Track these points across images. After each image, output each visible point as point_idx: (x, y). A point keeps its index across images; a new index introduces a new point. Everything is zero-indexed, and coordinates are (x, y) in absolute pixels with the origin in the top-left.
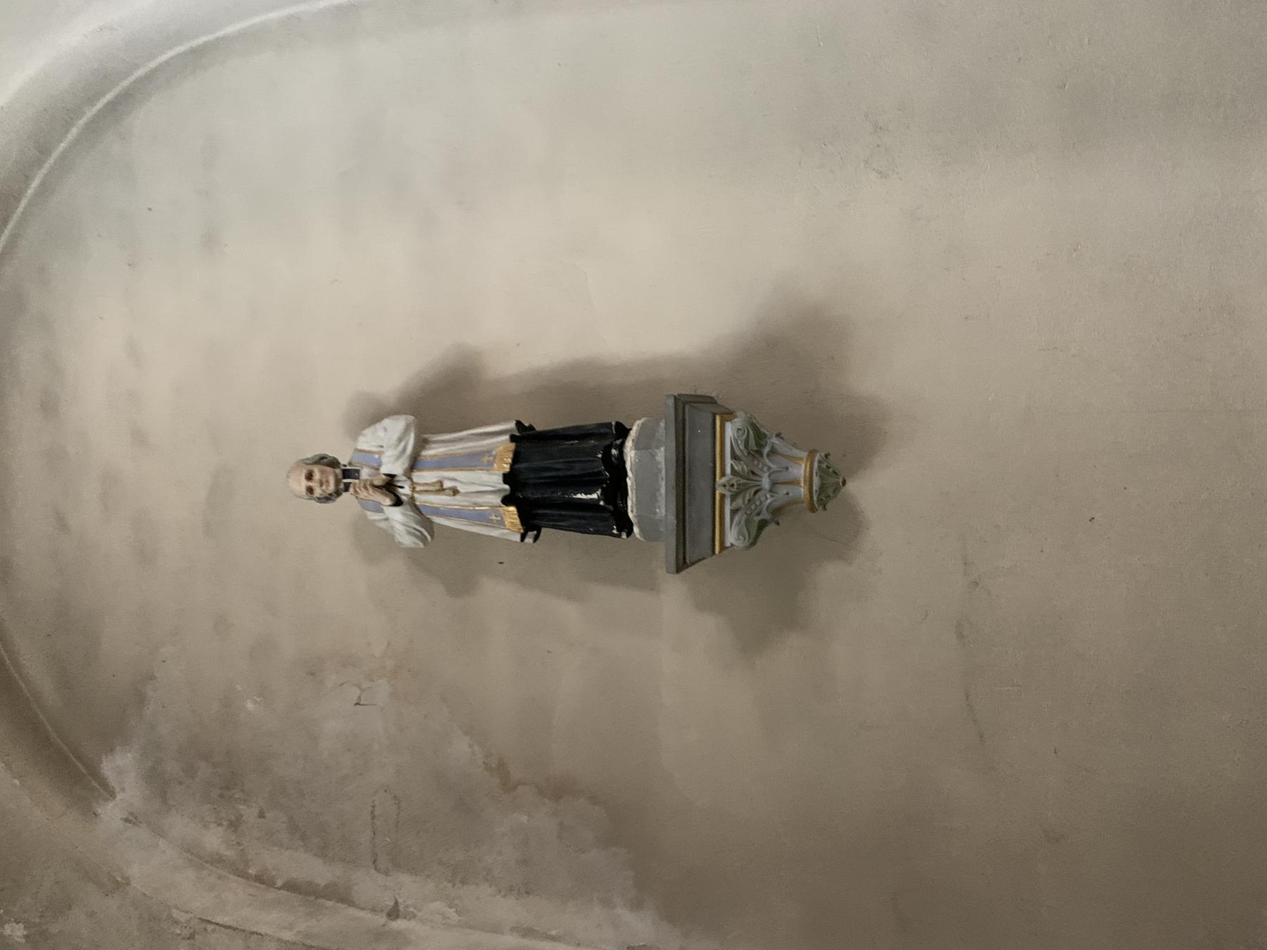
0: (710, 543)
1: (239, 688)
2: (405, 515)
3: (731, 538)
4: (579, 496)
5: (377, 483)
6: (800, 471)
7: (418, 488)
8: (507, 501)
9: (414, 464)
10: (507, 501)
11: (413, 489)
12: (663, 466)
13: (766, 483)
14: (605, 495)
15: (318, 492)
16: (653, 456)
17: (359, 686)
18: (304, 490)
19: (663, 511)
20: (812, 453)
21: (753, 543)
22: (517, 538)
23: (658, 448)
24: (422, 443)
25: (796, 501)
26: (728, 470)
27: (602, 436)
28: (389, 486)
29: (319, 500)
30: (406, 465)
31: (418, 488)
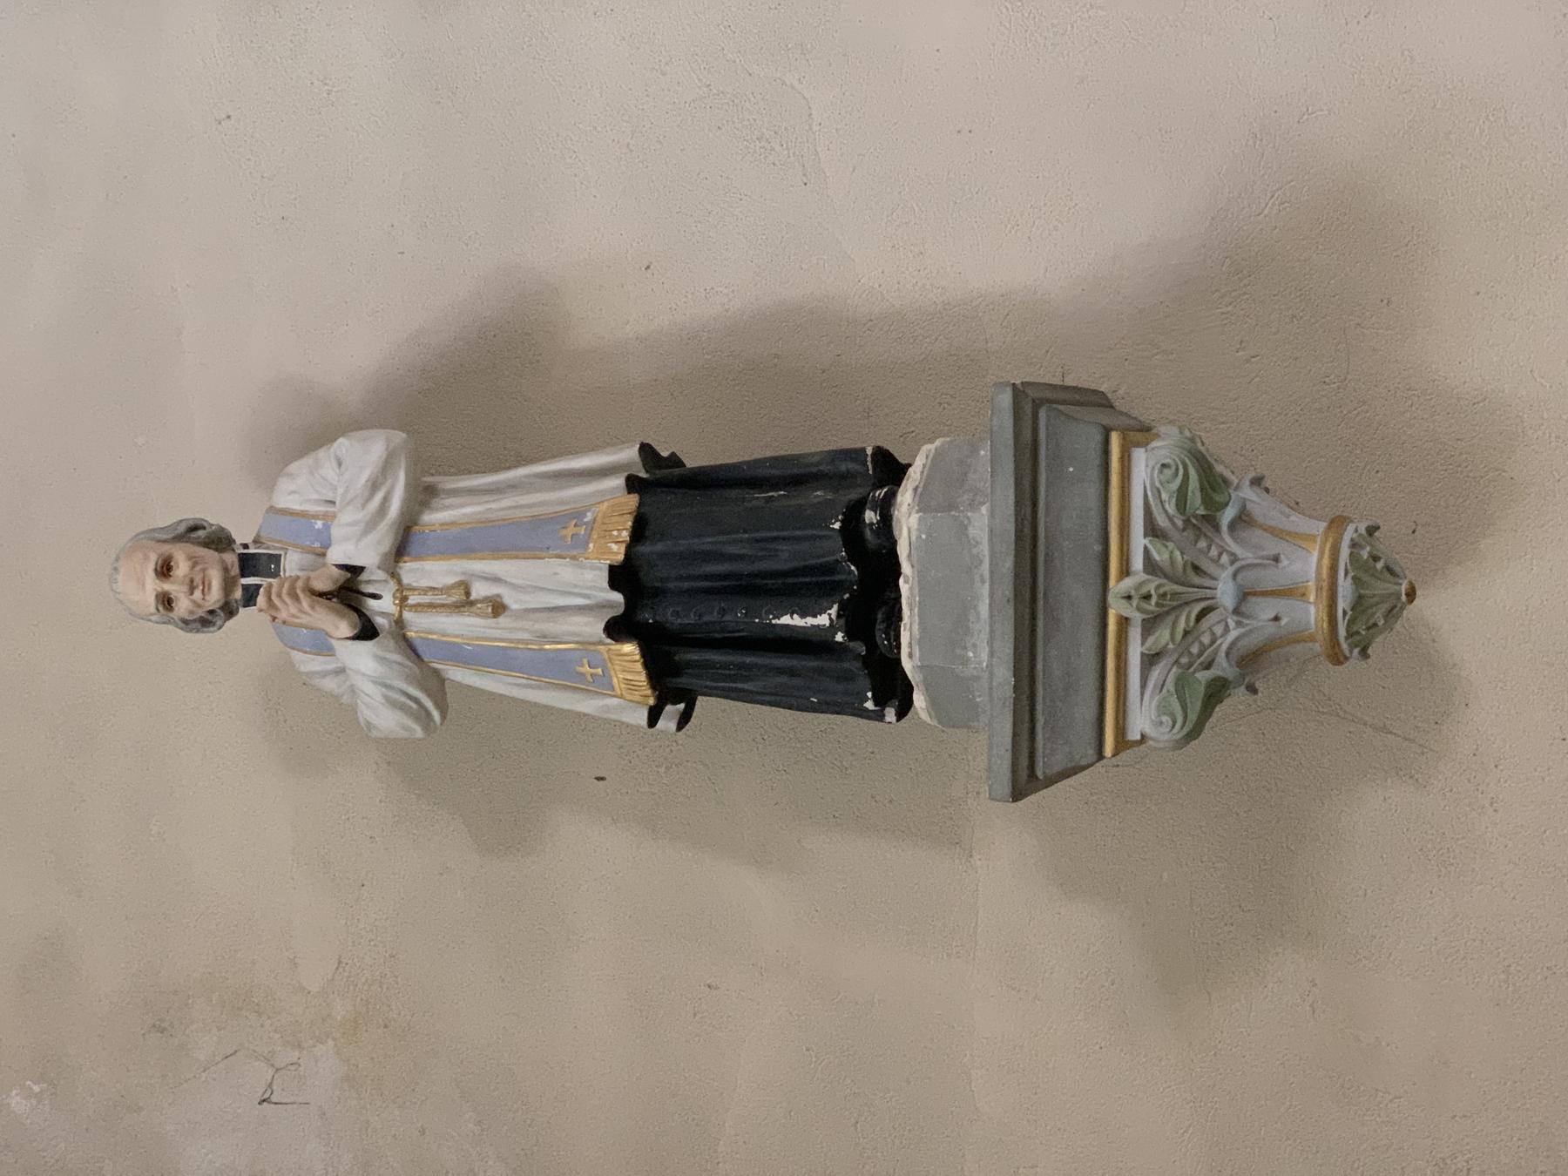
0: (1089, 733)
3: (1141, 721)
4: (786, 620)
5: (320, 586)
6: (1307, 565)
8: (617, 629)
10: (617, 629)
12: (985, 548)
13: (1225, 593)
16: (963, 528)
17: (268, 1060)
19: (984, 655)
20: (1337, 523)
21: (1194, 733)
22: (641, 717)
23: (973, 506)
24: (423, 495)
26: (1138, 563)
28: (348, 592)
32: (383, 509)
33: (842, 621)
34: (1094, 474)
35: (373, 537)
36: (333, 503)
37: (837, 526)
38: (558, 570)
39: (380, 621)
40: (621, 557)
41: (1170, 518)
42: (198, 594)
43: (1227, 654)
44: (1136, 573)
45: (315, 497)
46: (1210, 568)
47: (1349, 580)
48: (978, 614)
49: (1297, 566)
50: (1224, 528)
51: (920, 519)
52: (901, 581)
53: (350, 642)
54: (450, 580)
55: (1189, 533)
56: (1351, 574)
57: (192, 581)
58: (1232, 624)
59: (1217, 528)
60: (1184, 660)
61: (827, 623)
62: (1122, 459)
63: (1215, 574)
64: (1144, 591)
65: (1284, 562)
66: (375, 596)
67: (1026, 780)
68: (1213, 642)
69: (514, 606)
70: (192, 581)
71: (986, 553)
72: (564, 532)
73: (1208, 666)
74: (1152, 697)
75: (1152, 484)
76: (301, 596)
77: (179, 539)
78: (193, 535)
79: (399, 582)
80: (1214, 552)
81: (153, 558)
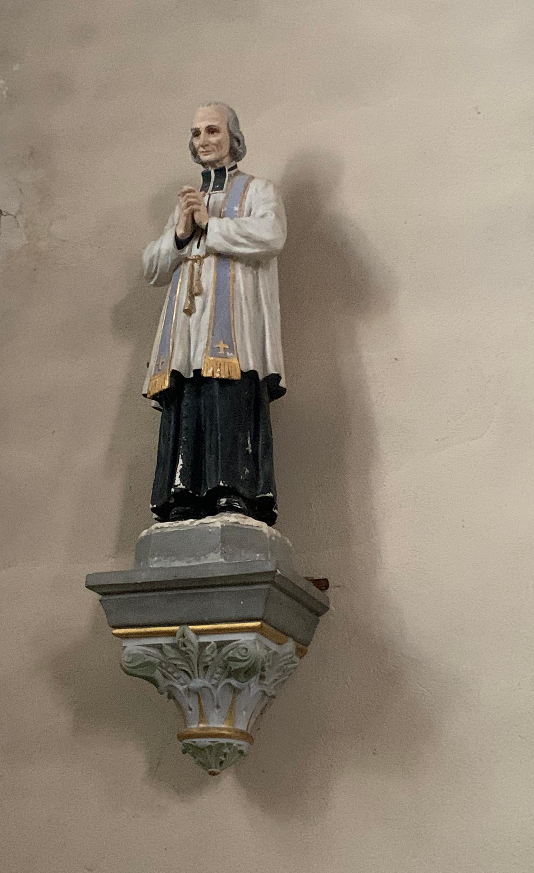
0: (124, 622)
1: (16, 68)
2: (168, 253)
3: (132, 646)
4: (181, 462)
5: (196, 216)
6: (217, 722)
7: (196, 265)
8: (175, 375)
9: (224, 257)
10: (175, 375)
11: (195, 260)
12: (203, 561)
13: (197, 683)
14: (181, 495)
15: (197, 142)
16: (213, 549)
17: (20, 212)
18: (197, 125)
19: (155, 566)
20: (246, 736)
21: (127, 673)
22: (145, 392)
23: (224, 554)
24: (254, 263)
25: (185, 722)
26: (203, 639)
27: (254, 480)
28: (198, 231)
29: (192, 144)
30: (219, 249)
31: (196, 265)
32: (236, 244)
33: (178, 491)
34: (241, 614)
35: (221, 240)
36: (249, 214)
37: (221, 484)
38: (203, 342)
39: (187, 248)
40: (205, 375)
41: (227, 653)
42: (201, 149)
43: (169, 685)
44: (198, 639)
45: (253, 202)
46: (209, 673)
47: (209, 744)
48: (173, 561)
49: (216, 718)
50: (227, 681)
51: (218, 528)
52: (192, 520)
53: (173, 235)
54: (204, 285)
55: (221, 663)
56: (213, 744)
57: (207, 145)
58: (185, 687)
59: (229, 677)
60: (164, 665)
61: (176, 484)
62: (248, 628)
63: (206, 678)
64: (187, 644)
65: (217, 711)
66: (198, 246)
67: (106, 590)
68: (175, 678)
69: (191, 319)
70: (207, 145)
71: (202, 563)
72: (222, 343)
73: (165, 676)
74: (144, 651)
75: (240, 644)
76: (189, 208)
77: (231, 134)
78: (234, 140)
79: (204, 257)
80: (216, 676)
81: (215, 123)
